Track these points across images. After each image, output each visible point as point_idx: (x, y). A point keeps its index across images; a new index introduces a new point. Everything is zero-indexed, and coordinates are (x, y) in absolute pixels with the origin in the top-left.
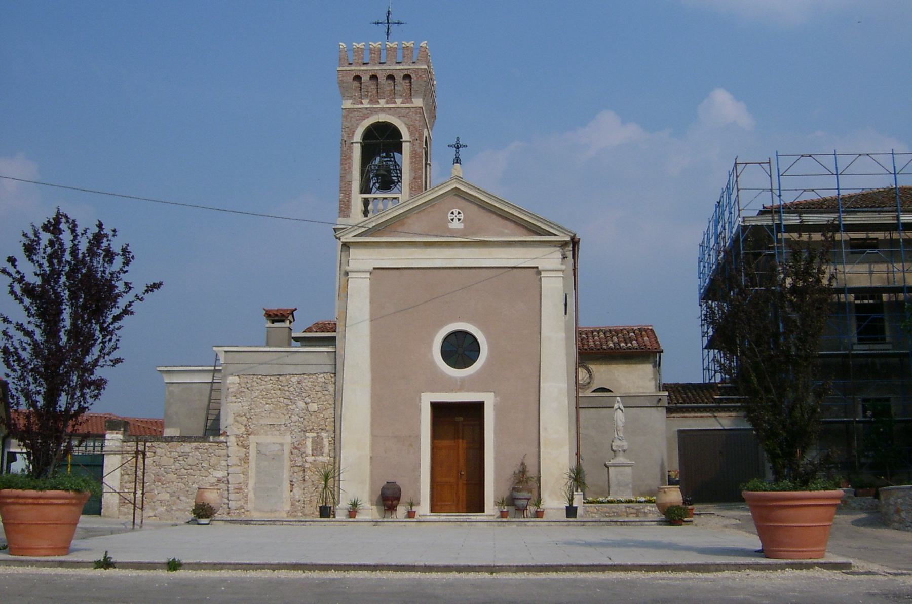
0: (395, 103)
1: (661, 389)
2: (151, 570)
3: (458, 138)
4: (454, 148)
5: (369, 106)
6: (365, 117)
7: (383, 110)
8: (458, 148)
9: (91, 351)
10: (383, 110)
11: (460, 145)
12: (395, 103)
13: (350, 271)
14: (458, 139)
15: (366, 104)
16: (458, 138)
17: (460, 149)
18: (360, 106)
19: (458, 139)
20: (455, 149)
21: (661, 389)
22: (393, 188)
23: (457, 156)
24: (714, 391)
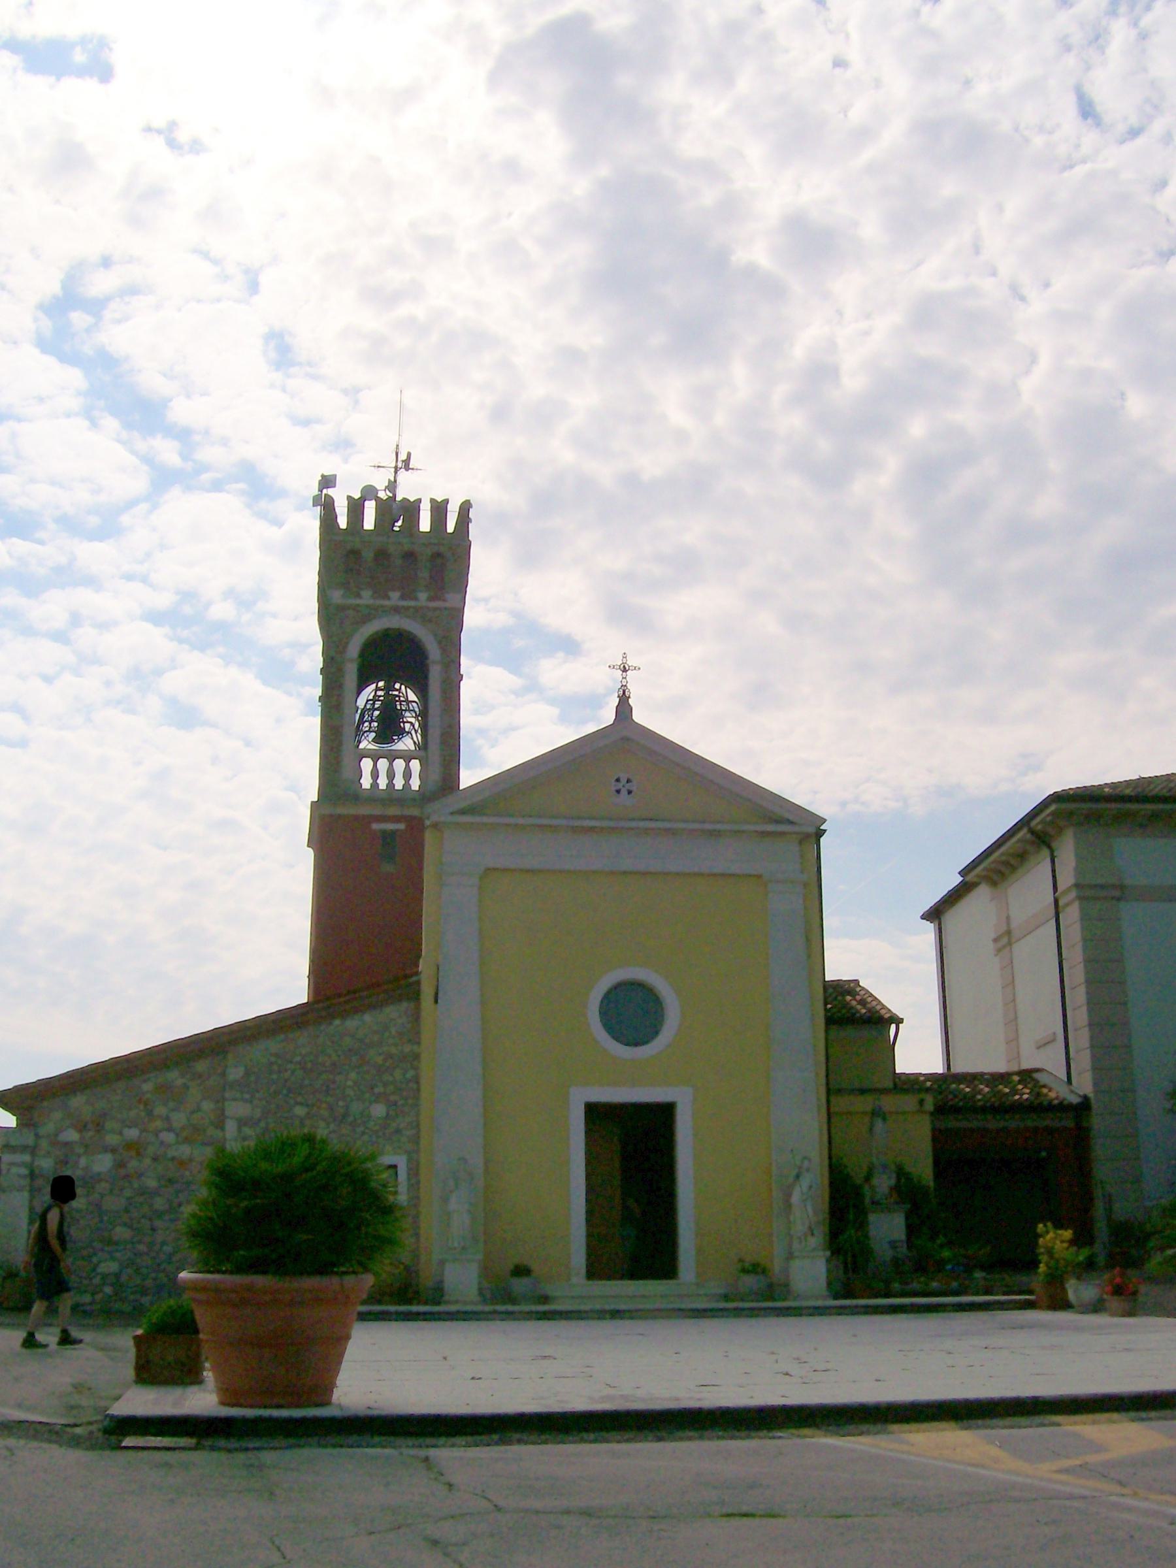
0: (416, 599)
1: (951, 1123)
2: (351, 1434)
3: (625, 654)
4: (619, 670)
5: (371, 602)
6: (365, 619)
7: (396, 610)
8: (625, 670)
9: (871, 1259)
10: (396, 610)
11: (629, 667)
12: (416, 599)
13: (940, 924)
14: (625, 656)
15: (367, 598)
16: (625, 654)
17: (628, 673)
18: (358, 601)
19: (625, 656)
20: (621, 672)
21: (951, 1123)
22: (396, 741)
23: (624, 684)
24: (406, 977)
